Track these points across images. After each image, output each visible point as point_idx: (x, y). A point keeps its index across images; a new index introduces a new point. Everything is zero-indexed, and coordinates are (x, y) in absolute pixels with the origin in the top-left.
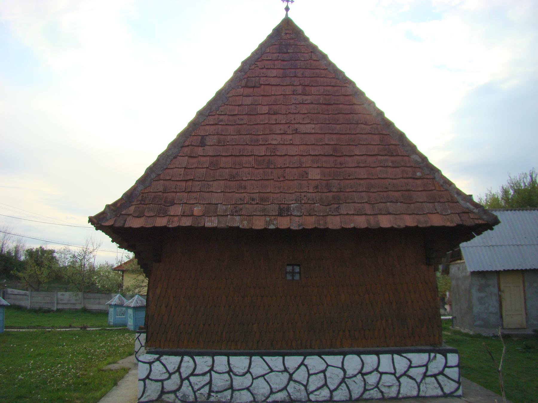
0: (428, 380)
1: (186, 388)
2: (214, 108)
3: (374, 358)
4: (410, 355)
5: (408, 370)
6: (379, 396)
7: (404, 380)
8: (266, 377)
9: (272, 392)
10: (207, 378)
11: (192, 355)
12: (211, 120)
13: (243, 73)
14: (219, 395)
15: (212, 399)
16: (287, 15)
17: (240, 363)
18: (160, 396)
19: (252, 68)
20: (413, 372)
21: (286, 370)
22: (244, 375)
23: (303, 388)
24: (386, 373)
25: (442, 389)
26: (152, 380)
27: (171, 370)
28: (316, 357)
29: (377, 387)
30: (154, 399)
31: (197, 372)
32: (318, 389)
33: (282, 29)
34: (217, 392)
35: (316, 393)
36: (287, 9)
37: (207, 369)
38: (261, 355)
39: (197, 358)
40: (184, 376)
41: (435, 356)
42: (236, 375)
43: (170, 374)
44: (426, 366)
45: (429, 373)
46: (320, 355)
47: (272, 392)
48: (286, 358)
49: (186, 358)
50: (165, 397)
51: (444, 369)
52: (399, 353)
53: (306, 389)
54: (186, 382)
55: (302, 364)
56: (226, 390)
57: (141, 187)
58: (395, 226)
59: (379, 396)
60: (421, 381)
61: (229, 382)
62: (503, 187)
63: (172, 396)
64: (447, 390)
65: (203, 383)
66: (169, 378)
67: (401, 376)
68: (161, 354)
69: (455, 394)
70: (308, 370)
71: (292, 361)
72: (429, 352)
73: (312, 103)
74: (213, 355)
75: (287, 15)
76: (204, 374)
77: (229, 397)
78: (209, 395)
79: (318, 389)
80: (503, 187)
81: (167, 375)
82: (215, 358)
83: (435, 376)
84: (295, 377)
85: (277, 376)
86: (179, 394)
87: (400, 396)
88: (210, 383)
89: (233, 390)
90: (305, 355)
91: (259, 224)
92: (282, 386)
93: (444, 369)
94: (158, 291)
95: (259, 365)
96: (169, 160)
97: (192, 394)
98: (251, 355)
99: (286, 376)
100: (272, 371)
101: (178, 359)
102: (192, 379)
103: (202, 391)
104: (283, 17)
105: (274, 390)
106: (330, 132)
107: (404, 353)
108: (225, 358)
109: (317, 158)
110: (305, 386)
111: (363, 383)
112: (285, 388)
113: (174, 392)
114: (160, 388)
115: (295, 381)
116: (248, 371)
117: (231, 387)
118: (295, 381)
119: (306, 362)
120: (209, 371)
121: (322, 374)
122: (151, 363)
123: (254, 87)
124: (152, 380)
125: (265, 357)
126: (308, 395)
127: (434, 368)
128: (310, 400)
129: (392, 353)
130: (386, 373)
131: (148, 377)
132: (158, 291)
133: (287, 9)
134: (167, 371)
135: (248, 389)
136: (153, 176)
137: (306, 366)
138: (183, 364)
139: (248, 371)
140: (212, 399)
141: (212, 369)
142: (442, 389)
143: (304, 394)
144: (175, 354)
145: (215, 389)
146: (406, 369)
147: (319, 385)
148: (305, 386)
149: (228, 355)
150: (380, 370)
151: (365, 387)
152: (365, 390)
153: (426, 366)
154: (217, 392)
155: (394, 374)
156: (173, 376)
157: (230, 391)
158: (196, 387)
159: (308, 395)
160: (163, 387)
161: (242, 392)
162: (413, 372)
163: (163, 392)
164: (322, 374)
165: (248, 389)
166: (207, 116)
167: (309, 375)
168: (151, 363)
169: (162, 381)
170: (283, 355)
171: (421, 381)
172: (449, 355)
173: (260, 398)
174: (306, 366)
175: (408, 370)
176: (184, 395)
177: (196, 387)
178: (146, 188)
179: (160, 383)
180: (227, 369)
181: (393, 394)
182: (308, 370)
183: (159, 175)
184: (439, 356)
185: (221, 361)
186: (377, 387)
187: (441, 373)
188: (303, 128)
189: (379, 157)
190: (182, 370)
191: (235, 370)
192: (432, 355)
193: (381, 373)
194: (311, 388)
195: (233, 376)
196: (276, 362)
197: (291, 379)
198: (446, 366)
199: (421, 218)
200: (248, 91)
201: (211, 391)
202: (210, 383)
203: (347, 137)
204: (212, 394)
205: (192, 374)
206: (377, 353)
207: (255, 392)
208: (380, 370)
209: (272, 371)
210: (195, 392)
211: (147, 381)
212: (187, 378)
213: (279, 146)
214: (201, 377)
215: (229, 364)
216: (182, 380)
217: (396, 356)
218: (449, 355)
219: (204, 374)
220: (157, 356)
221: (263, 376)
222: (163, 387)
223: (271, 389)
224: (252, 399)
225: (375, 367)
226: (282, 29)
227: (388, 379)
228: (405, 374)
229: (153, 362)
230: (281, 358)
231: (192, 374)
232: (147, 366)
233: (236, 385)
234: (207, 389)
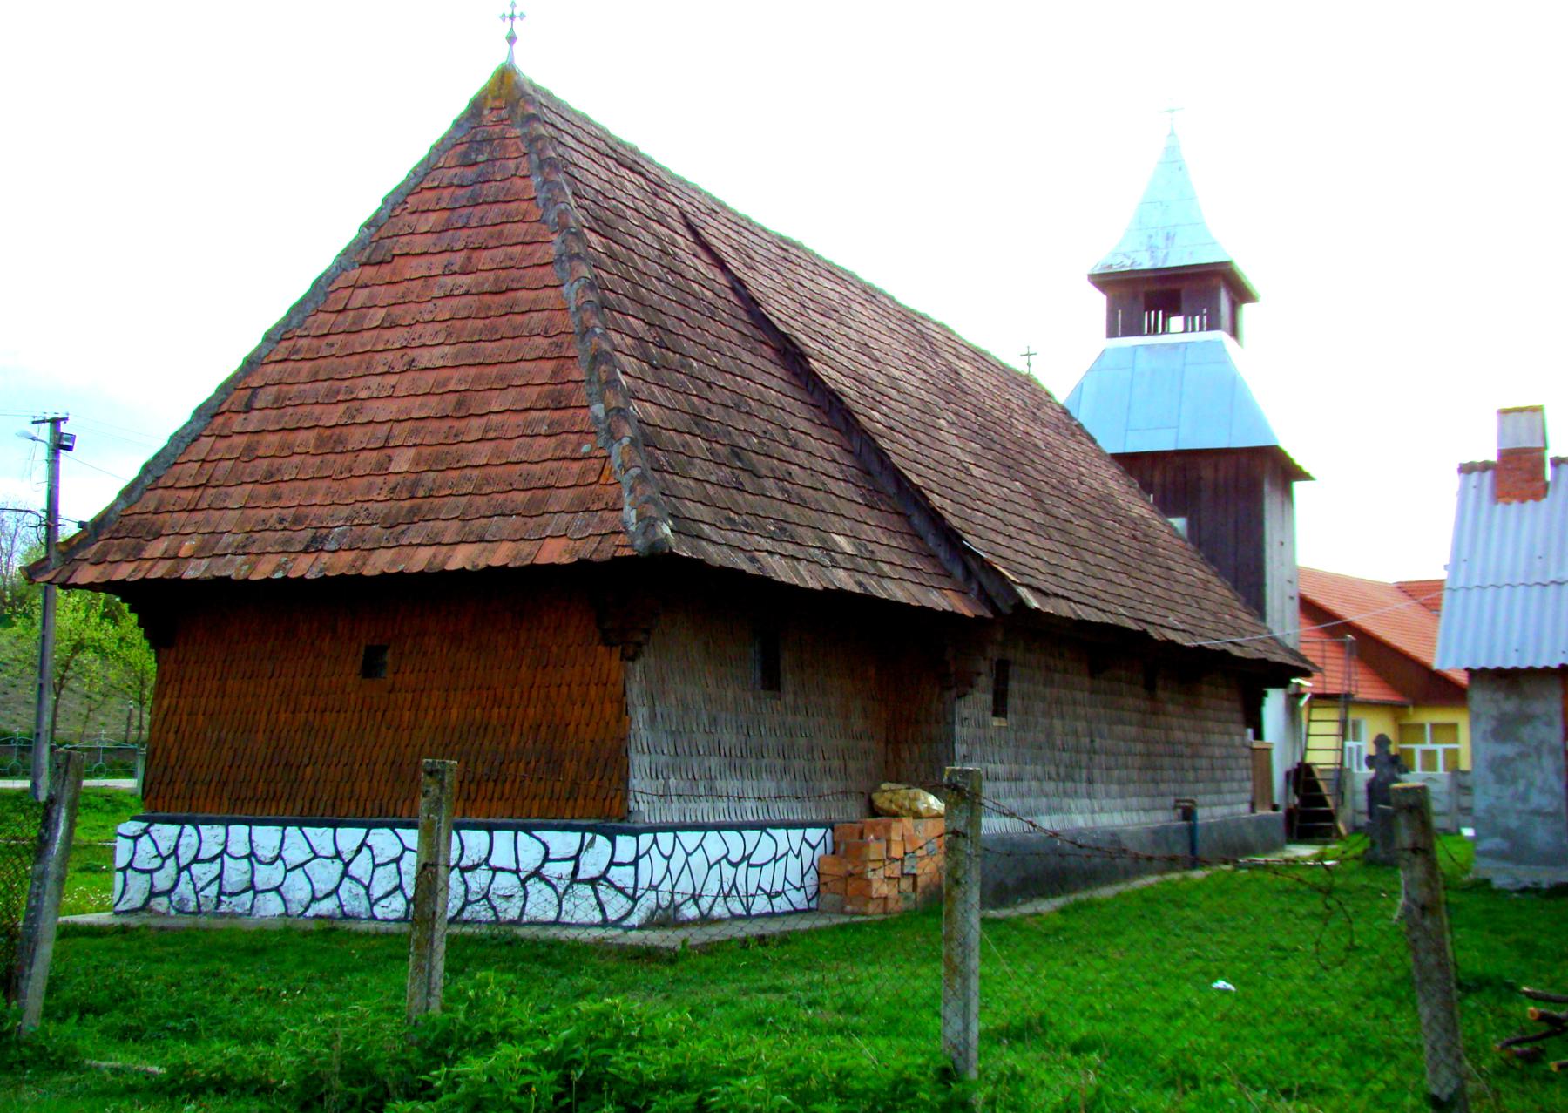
1: (185, 888)
2: (295, 322)
3: (483, 835)
4: (546, 835)
5: (542, 866)
6: (490, 915)
7: (534, 886)
9: (314, 899)
10: (216, 867)
11: (196, 823)
12: (282, 350)
14: (234, 900)
15: (223, 908)
16: (511, 54)
17: (267, 837)
18: (147, 901)
19: (397, 212)
20: (551, 869)
21: (338, 855)
22: (272, 863)
23: (363, 891)
24: (503, 870)
25: (603, 911)
26: (136, 870)
28: (387, 831)
29: (486, 896)
30: (139, 905)
31: (203, 855)
32: (388, 894)
33: (485, 98)
34: (231, 894)
35: (383, 902)
36: (512, 39)
37: (218, 849)
39: (204, 828)
40: (183, 862)
41: (593, 840)
42: (261, 862)
43: (165, 859)
45: (581, 876)
46: (392, 826)
47: (314, 899)
48: (339, 830)
52: (528, 830)
53: (368, 895)
54: (185, 874)
55: (363, 844)
56: (244, 891)
59: (490, 915)
60: (565, 893)
61: (248, 876)
62: (1304, 476)
63: (164, 900)
64: (612, 915)
65: (211, 876)
66: (161, 867)
67: (528, 878)
69: (625, 923)
71: (349, 837)
72: (583, 829)
73: (467, 293)
74: (227, 823)
75: (511, 54)
76: (212, 860)
77: (248, 906)
78: (219, 902)
79: (388, 894)
80: (1304, 476)
81: (158, 861)
82: (231, 828)
83: (592, 882)
84: (353, 869)
85: (324, 866)
86: (175, 897)
87: (525, 919)
88: (220, 876)
90: (370, 826)
92: (331, 886)
95: (297, 843)
96: (183, 446)
97: (193, 897)
98: (284, 824)
100: (316, 856)
101: (176, 829)
102: (195, 868)
103: (206, 892)
105: (319, 895)
106: (471, 361)
108: (244, 829)
110: (367, 888)
112: (336, 891)
113: (168, 893)
115: (352, 878)
116: (279, 856)
117: (252, 886)
118: (352, 878)
119: (370, 841)
120: (220, 855)
122: (136, 838)
123: (380, 263)
124: (136, 870)
125: (306, 829)
126: (372, 905)
127: (589, 868)
129: (516, 828)
130: (503, 870)
131: (130, 865)
133: (512, 39)
134: (159, 854)
135: (277, 889)
136: (148, 481)
137: (370, 847)
138: (183, 841)
139: (279, 856)
140: (223, 908)
141: (224, 851)
142: (603, 911)
143: (365, 903)
145: (228, 889)
146: (538, 864)
148: (367, 888)
149: (250, 823)
150: (493, 862)
152: (467, 903)
154: (231, 894)
155: (517, 871)
156: (168, 862)
157: (251, 893)
158: (200, 885)
159: (372, 905)
160: (152, 885)
161: (268, 895)
162: (551, 869)
163: (153, 894)
164: (394, 865)
165: (277, 889)
166: (278, 342)
167: (375, 866)
168: (136, 838)
169: (151, 872)
170: (335, 825)
171: (565, 893)
172: (620, 839)
173: (296, 908)
175: (542, 866)
176: (181, 900)
177: (200, 885)
178: (130, 506)
179: (147, 877)
180: (248, 851)
181: (513, 913)
186: (486, 896)
187: (604, 876)
188: (425, 357)
190: (180, 852)
191: (259, 853)
192: (588, 836)
193: (495, 870)
194: (377, 892)
195: (256, 865)
196: (321, 837)
198: (611, 863)
201: (221, 892)
202: (220, 876)
203: (495, 370)
204: (223, 898)
205: (196, 860)
206: (490, 829)
207: (289, 896)
208: (493, 862)
209: (316, 856)
210: (197, 893)
211: (129, 871)
212: (188, 867)
213: (368, 403)
214: (207, 865)
215: (251, 841)
216: (180, 870)
217: (521, 835)
218: (620, 839)
219: (212, 860)
221: (302, 865)
222: (152, 885)
224: (282, 910)
225: (484, 856)
226: (485, 98)
227: (506, 882)
228: (537, 873)
229: (140, 836)
230: (331, 830)
231: (196, 860)
232: (130, 843)
233: (260, 883)
234: (214, 888)
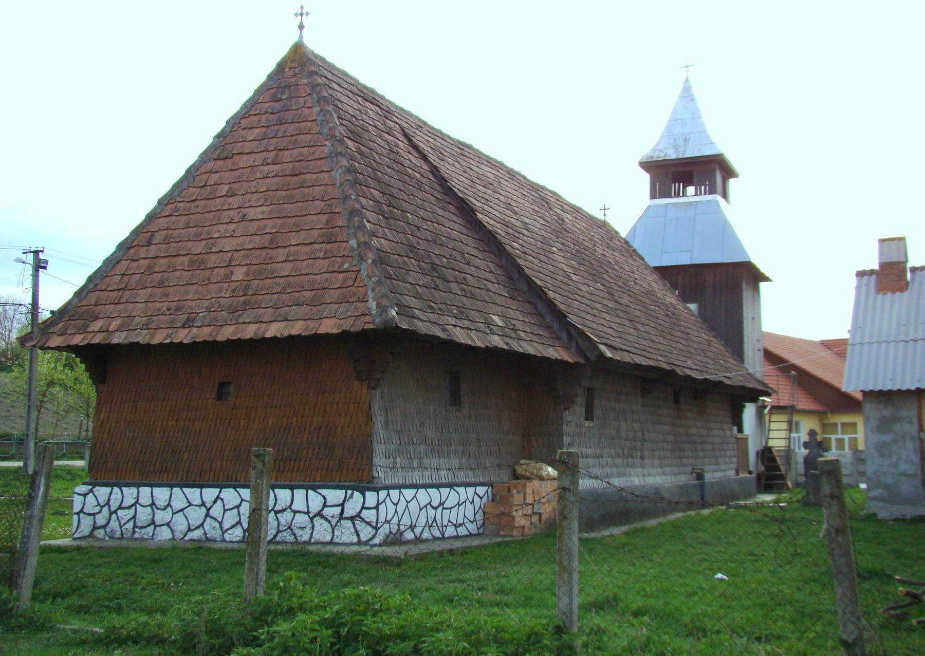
0: (344, 522)
1: (114, 524)
2: (176, 193)
4: (325, 492)
5: (322, 509)
6: (292, 538)
7: (318, 521)
8: (185, 511)
9: (190, 530)
10: (132, 511)
11: (120, 487)
13: (221, 139)
14: (143, 531)
16: (301, 35)
20: (328, 512)
21: (203, 504)
22: (164, 509)
23: (218, 525)
25: (358, 535)
26: (86, 514)
27: (102, 504)
28: (232, 490)
29: (290, 528)
30: (87, 534)
33: (286, 62)
34: (141, 528)
35: (230, 532)
36: (301, 27)
37: (133, 501)
38: (181, 486)
39: (124, 489)
40: (113, 509)
42: (158, 509)
43: (102, 507)
44: (342, 505)
45: (345, 515)
46: (235, 487)
47: (190, 530)
49: (116, 489)
50: (96, 532)
51: (361, 511)
52: (314, 489)
53: (221, 527)
54: (114, 516)
55: (218, 497)
56: (148, 526)
57: (76, 301)
58: (278, 336)
59: (292, 538)
60: (336, 525)
61: (151, 517)
63: (102, 531)
66: (100, 512)
67: (314, 516)
68: (94, 485)
70: (224, 506)
71: (210, 494)
72: (346, 488)
73: (276, 176)
74: (138, 486)
75: (301, 35)
76: (130, 507)
78: (134, 532)
81: (98, 509)
83: (352, 519)
85: (195, 510)
86: (108, 530)
87: (313, 540)
88: (134, 517)
89: (156, 526)
90: (221, 487)
91: (159, 338)
92: (199, 522)
93: (361, 511)
94: (102, 416)
95: (179, 497)
96: (111, 266)
97: (118, 529)
98: (172, 486)
99: (204, 510)
100: (190, 505)
101: (108, 489)
102: (120, 512)
104: (294, 39)
105: (192, 527)
107: (320, 488)
109: (250, 252)
110: (220, 523)
111: (276, 523)
112: (202, 525)
114: (92, 523)
115: (212, 517)
116: (169, 505)
117: (153, 522)
118: (212, 517)
119: (222, 496)
120: (134, 504)
121: (236, 510)
122: (85, 495)
123: (226, 158)
124: (86, 514)
126: (223, 533)
128: (224, 540)
129: (307, 488)
131: (82, 511)
132: (102, 416)
133: (301, 27)
134: (99, 504)
135: (168, 524)
137: (222, 500)
138: (113, 496)
139: (169, 505)
140: (136, 536)
141: (137, 502)
142: (358, 535)
143: (219, 532)
144: (106, 485)
147: (233, 523)
148: (220, 523)
149: (151, 486)
150: (293, 507)
151: (292, 530)
152: (279, 531)
153: (342, 505)
154: (141, 528)
155: (308, 513)
157: (152, 526)
159: (223, 533)
160: (95, 522)
162: (328, 512)
163: (95, 528)
164: (236, 510)
165: (168, 524)
167: (225, 510)
168: (85, 495)
169: (94, 515)
170: (201, 487)
171: (336, 525)
172: (368, 494)
173: (179, 535)
174: (222, 500)
175: (322, 509)
176: (112, 531)
179: (92, 517)
181: (306, 537)
182: (224, 506)
183: (97, 285)
184: (357, 494)
185: (145, 491)
186: (290, 528)
187: (358, 515)
188: (252, 213)
189: (316, 246)
190: (111, 502)
191: (157, 503)
192: (349, 492)
193: (295, 512)
194: (226, 525)
196: (193, 494)
197: (207, 515)
198: (363, 508)
199: (312, 324)
200: (220, 163)
201: (135, 526)
202: (134, 517)
205: (120, 507)
206: (292, 488)
207: (175, 528)
209: (190, 505)
210: (121, 527)
211: (81, 515)
212: (115, 512)
215: (152, 496)
216: (111, 514)
217: (310, 492)
218: (368, 494)
219: (130, 507)
220: (90, 487)
221: (182, 510)
222: (95, 522)
223: (189, 525)
226: (286, 62)
227: (301, 519)
228: (319, 514)
231: (120, 507)
232: (82, 498)
233: (158, 520)
